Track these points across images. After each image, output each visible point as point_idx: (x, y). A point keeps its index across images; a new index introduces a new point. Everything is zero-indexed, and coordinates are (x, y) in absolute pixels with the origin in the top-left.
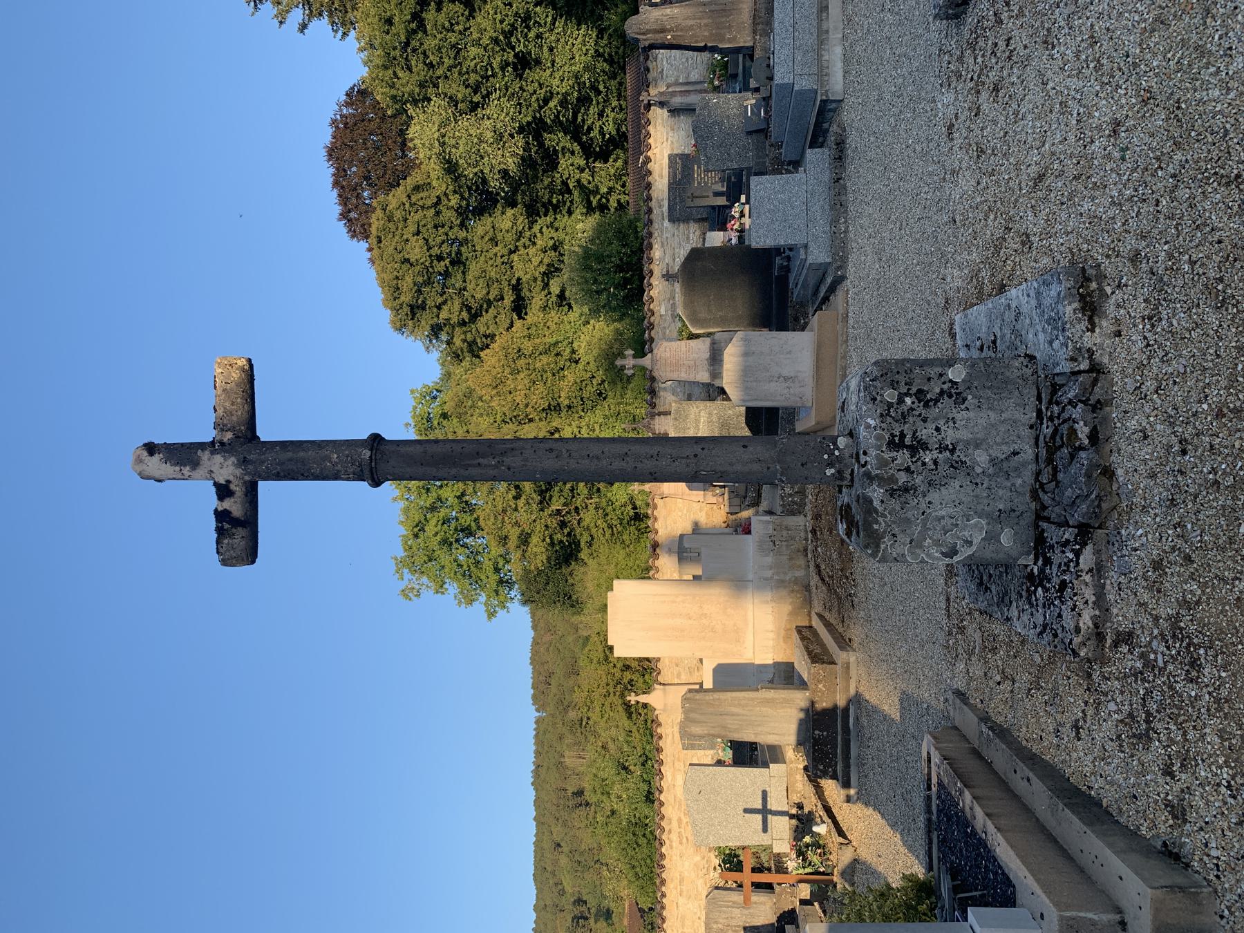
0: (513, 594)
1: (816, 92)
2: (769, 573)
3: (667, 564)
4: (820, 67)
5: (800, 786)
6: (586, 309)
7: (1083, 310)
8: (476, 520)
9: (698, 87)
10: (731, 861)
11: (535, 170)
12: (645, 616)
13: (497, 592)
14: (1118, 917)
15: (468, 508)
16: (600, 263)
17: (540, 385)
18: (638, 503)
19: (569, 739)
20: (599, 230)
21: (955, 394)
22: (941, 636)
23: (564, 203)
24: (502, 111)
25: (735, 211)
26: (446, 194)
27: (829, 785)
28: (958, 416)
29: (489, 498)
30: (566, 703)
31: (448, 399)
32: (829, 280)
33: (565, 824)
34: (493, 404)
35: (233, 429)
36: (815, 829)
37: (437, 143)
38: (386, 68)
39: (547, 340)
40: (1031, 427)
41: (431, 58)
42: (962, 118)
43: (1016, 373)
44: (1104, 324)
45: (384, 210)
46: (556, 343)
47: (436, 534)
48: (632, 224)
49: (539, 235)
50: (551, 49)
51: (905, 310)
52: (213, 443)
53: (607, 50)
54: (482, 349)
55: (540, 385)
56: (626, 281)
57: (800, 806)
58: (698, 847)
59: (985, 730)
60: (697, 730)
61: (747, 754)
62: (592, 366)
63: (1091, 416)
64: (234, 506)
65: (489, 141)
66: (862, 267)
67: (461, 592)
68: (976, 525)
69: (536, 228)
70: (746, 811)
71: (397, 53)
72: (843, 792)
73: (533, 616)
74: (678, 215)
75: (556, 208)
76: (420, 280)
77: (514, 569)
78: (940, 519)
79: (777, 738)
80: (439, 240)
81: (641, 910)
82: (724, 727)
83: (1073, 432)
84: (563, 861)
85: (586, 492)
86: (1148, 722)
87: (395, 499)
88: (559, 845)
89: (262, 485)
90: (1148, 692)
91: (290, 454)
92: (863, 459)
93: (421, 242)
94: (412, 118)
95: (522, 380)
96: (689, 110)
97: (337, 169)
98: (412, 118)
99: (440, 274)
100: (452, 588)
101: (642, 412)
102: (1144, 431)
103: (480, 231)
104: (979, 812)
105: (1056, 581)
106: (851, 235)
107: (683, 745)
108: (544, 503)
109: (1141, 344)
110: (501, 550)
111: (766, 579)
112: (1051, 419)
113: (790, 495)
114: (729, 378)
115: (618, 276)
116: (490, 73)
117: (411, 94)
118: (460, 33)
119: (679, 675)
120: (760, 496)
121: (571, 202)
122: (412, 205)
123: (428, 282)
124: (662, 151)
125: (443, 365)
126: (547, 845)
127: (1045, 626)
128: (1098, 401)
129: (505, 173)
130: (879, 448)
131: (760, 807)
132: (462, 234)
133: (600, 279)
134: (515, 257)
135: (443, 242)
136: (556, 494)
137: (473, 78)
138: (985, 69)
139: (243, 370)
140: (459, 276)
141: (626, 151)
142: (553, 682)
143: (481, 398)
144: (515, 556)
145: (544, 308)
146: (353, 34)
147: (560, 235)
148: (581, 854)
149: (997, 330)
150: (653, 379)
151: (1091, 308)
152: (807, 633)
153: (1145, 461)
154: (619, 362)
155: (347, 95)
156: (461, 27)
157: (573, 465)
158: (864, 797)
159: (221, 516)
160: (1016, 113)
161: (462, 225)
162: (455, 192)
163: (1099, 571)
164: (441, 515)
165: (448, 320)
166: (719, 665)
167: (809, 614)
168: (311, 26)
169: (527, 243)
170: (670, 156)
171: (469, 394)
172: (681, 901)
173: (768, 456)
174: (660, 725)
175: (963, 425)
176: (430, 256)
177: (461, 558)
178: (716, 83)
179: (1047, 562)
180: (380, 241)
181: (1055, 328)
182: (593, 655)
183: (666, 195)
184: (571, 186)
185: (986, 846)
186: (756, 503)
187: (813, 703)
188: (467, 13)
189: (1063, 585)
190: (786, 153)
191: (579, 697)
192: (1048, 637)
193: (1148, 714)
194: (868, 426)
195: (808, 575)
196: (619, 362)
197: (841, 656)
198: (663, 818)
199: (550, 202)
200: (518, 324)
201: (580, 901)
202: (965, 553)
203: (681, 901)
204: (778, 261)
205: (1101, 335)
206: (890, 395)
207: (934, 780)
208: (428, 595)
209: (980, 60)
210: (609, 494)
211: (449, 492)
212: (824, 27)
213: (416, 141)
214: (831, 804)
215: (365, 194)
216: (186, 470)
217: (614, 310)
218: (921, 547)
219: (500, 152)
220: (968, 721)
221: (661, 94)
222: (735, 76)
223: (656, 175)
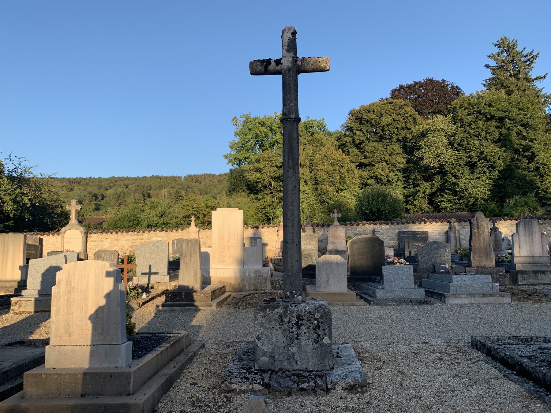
0: (235, 166)
1: (449, 292)
2: (247, 275)
3: (250, 232)
4: (459, 294)
5: (160, 288)
6: (360, 195)
7: (350, 386)
8: (267, 149)
9: (458, 244)
10: (130, 260)
11: (424, 172)
12: (229, 223)
13: (236, 159)
14: (131, 393)
15: (272, 145)
16: (381, 202)
17: (326, 176)
18: (275, 220)
19: (172, 191)
20: (396, 201)
21: (318, 340)
22: (225, 340)
23: (409, 185)
24: (449, 156)
25: (402, 260)
26: (412, 132)
27: (163, 299)
28: (310, 341)
29: (276, 154)
30: (188, 189)
31: (320, 135)
32: (369, 298)
33: (136, 190)
34: (318, 155)
35: (302, 65)
36: (144, 294)
37: (435, 128)
38: (469, 104)
39: (347, 179)
40: (306, 368)
41: (474, 124)
42: (430, 347)
43: (327, 363)
44: (345, 394)
45: (404, 105)
46: (345, 183)
47: (260, 132)
48: (399, 215)
49: (394, 174)
50: (479, 178)
51: (355, 327)
52: (296, 57)
53: (479, 203)
54: (342, 150)
55: (326, 176)
56: (373, 213)
57: (152, 288)
58: (132, 247)
59: (191, 354)
60: (184, 245)
61: (174, 266)
62: (336, 199)
63: (311, 389)
64: (272, 66)
65: (437, 151)
66: (374, 311)
67: (235, 143)
68: (269, 347)
69: (397, 173)
70: (150, 266)
71: (476, 109)
72: (160, 304)
73: (225, 174)
74: (401, 236)
75: (406, 181)
76: (373, 122)
77: (246, 166)
78: (271, 334)
79: (181, 278)
80: (391, 129)
81: (102, 223)
82: (185, 256)
83: (305, 382)
84: (120, 190)
85: (280, 197)
86: (199, 406)
87: (275, 113)
88: (127, 187)
89: (281, 76)
90: (210, 407)
91: (292, 87)
92: (293, 305)
93: (390, 122)
94: (446, 116)
95: (329, 168)
96: (448, 240)
97: (423, 84)
98: (446, 116)
99: (376, 130)
100: (237, 139)
101: (315, 221)
102: (305, 406)
103: (396, 148)
104: (162, 349)
105: (249, 376)
106: (388, 307)
107: (174, 240)
108: (275, 178)
109: (337, 405)
110: (253, 160)
111: (244, 273)
112: (309, 375)
113: (279, 283)
114: (327, 257)
115: (375, 210)
116: (467, 151)
117: (457, 116)
118: (486, 137)
119: (203, 238)
120: (279, 271)
121: (410, 188)
122: (407, 117)
123: (372, 125)
124: (429, 228)
125: (335, 132)
126: (127, 182)
127: (232, 373)
128: (316, 391)
129: (422, 158)
130: (298, 311)
131: (152, 271)
132: (394, 140)
133: (374, 202)
134: (384, 164)
135: (390, 131)
136: (278, 184)
137: (465, 143)
138: (449, 355)
139: (325, 68)
140: (375, 139)
141: (433, 212)
142: (197, 184)
143: (320, 150)
144: (251, 166)
145: (361, 177)
146: (485, 89)
147: (394, 184)
148: (123, 197)
149: (344, 358)
150: (329, 226)
151: (351, 389)
152: (223, 290)
153: (294, 406)
154: (335, 211)
155: (457, 87)
156: (488, 137)
157: (289, 196)
158: (158, 313)
159: (269, 61)
160: (430, 366)
161: (398, 140)
162: (413, 136)
163: (253, 391)
164: (269, 134)
165: (355, 135)
166: (209, 254)
167: (230, 291)
168: (488, 70)
169: (391, 169)
170: (427, 232)
171: (322, 145)
172: (109, 240)
173: (294, 274)
174: (182, 230)
175: (307, 343)
176: (384, 126)
177: (250, 143)
178: (459, 252)
179: (256, 374)
180: (390, 103)
181: (343, 376)
182: (209, 202)
183: (410, 230)
184: (417, 188)
185: (150, 351)
186: (276, 270)
187: (196, 292)
188: (495, 140)
189: (248, 379)
190: (425, 281)
191: (191, 196)
192: (228, 374)
193: (202, 406)
194: (306, 307)
195: (247, 291)
196: (335, 211)
197: (214, 303)
198: (143, 232)
199: (409, 179)
200: (354, 166)
201: (103, 197)
202: (259, 343)
203: (109, 240)
204: (378, 278)
205: (341, 392)
206: (318, 315)
207: (171, 335)
208: (234, 129)
209: (453, 353)
210: (278, 207)
211: (279, 137)
212: (476, 296)
213: (436, 119)
214: (155, 300)
215: (412, 96)
216: (286, 47)
217: (360, 208)
218: (261, 326)
219: (431, 156)
220: (194, 348)
221: (455, 228)
222: (462, 259)
223: (419, 226)
